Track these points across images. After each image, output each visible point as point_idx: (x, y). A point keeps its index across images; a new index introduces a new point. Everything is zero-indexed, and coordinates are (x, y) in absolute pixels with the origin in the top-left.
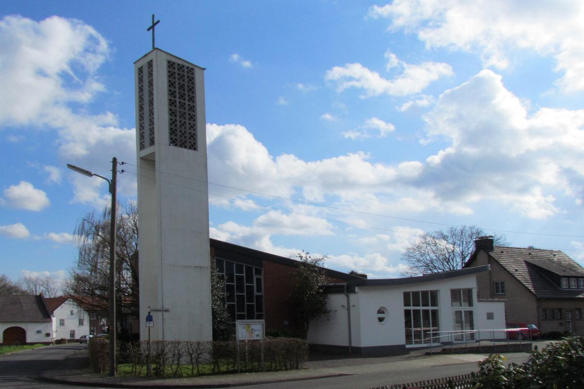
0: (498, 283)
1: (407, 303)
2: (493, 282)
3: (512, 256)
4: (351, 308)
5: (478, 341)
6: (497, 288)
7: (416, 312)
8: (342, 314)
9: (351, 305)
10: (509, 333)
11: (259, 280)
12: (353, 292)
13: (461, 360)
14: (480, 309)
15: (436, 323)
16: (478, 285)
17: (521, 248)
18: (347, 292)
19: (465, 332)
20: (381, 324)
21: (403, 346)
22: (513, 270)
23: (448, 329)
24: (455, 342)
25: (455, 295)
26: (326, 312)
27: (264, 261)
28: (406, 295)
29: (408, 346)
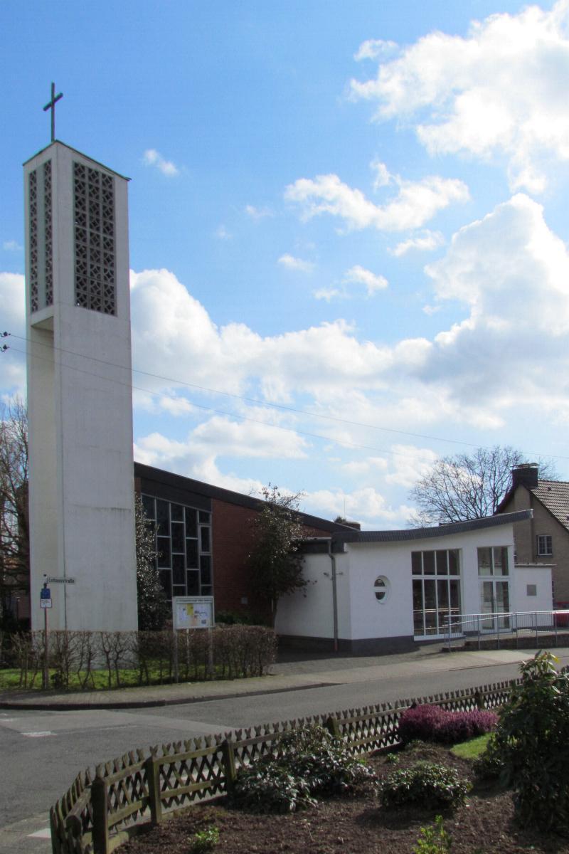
0: (543, 537)
4: (338, 576)
5: (514, 630)
10: (557, 617)
11: (205, 531)
12: (341, 551)
13: (489, 660)
14: (519, 578)
19: (498, 615)
21: (412, 637)
23: (473, 611)
25: (484, 556)
26: (302, 584)
27: (212, 500)
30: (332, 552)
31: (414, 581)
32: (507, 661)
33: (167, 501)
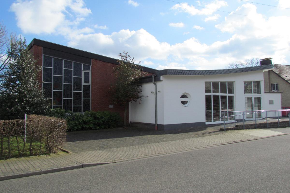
0: (274, 84)
1: (207, 91)
2: (271, 84)
3: (283, 69)
4: (158, 93)
5: (264, 119)
6: (274, 87)
7: (216, 98)
8: (152, 98)
9: (158, 90)
10: (283, 113)
11: (86, 75)
12: (159, 80)
13: (253, 136)
14: (265, 97)
15: (231, 106)
16: (264, 79)
17: (288, 65)
18: (155, 81)
19: (255, 112)
20: (183, 105)
21: (205, 123)
22: (285, 76)
23: (241, 107)
24: (246, 119)
25: (247, 88)
26: (139, 97)
27: (92, 60)
28: (207, 84)
29: (207, 123)
30: (155, 81)
31: (206, 96)
32: (263, 136)
33: (62, 59)
